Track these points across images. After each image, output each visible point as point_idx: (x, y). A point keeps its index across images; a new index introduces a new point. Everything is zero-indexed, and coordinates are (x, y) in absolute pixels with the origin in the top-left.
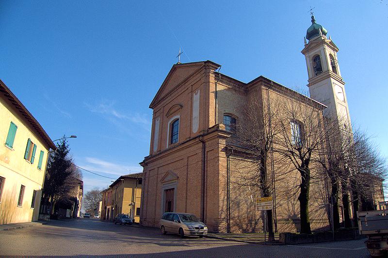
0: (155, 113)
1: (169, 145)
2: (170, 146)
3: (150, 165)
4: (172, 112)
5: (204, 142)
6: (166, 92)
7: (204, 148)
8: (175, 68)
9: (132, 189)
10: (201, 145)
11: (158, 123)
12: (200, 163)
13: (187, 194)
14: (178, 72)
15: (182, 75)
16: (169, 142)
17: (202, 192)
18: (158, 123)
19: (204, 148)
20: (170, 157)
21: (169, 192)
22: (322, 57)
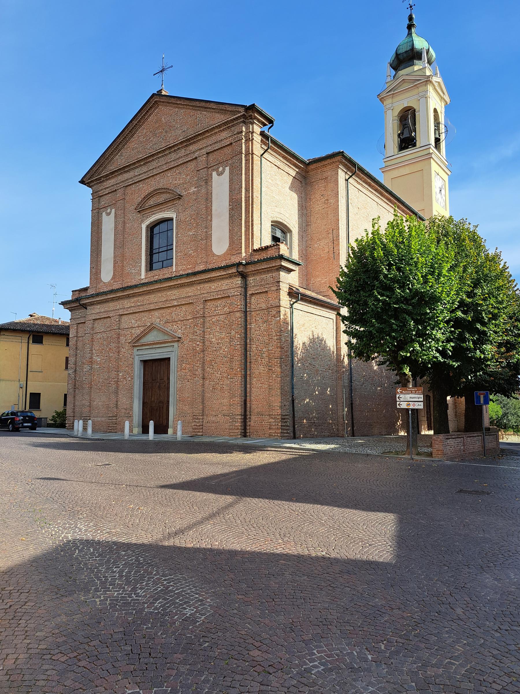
0: (96, 197)
1: (147, 271)
2: (151, 274)
3: (94, 311)
4: (151, 202)
5: (244, 276)
6: (120, 160)
7: (245, 287)
8: (156, 100)
9: (70, 298)
10: (238, 281)
11: (108, 222)
12: (164, 145)
13: (203, 370)
14: (163, 114)
15: (178, 124)
16: (146, 266)
17: (243, 366)
18: (108, 222)
19: (245, 287)
20: (153, 298)
21: (156, 372)
22: (419, 116)
